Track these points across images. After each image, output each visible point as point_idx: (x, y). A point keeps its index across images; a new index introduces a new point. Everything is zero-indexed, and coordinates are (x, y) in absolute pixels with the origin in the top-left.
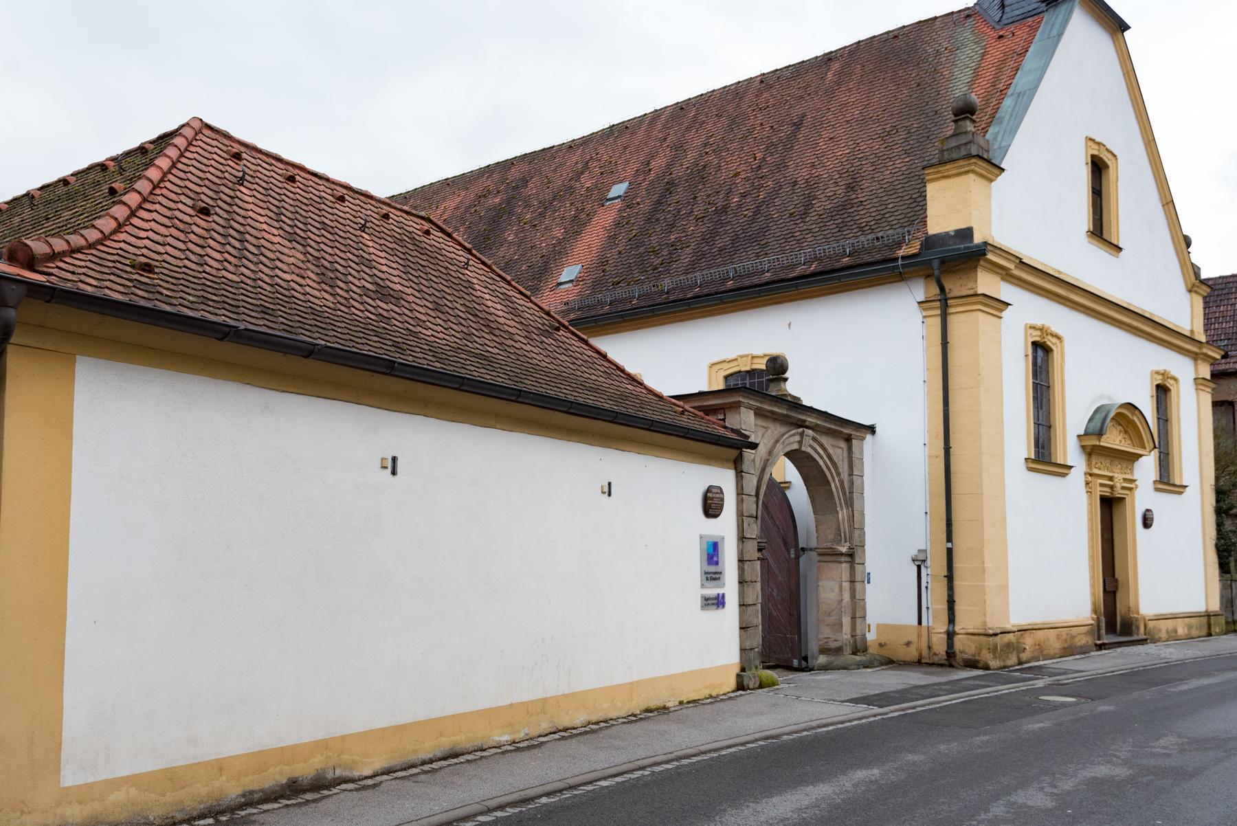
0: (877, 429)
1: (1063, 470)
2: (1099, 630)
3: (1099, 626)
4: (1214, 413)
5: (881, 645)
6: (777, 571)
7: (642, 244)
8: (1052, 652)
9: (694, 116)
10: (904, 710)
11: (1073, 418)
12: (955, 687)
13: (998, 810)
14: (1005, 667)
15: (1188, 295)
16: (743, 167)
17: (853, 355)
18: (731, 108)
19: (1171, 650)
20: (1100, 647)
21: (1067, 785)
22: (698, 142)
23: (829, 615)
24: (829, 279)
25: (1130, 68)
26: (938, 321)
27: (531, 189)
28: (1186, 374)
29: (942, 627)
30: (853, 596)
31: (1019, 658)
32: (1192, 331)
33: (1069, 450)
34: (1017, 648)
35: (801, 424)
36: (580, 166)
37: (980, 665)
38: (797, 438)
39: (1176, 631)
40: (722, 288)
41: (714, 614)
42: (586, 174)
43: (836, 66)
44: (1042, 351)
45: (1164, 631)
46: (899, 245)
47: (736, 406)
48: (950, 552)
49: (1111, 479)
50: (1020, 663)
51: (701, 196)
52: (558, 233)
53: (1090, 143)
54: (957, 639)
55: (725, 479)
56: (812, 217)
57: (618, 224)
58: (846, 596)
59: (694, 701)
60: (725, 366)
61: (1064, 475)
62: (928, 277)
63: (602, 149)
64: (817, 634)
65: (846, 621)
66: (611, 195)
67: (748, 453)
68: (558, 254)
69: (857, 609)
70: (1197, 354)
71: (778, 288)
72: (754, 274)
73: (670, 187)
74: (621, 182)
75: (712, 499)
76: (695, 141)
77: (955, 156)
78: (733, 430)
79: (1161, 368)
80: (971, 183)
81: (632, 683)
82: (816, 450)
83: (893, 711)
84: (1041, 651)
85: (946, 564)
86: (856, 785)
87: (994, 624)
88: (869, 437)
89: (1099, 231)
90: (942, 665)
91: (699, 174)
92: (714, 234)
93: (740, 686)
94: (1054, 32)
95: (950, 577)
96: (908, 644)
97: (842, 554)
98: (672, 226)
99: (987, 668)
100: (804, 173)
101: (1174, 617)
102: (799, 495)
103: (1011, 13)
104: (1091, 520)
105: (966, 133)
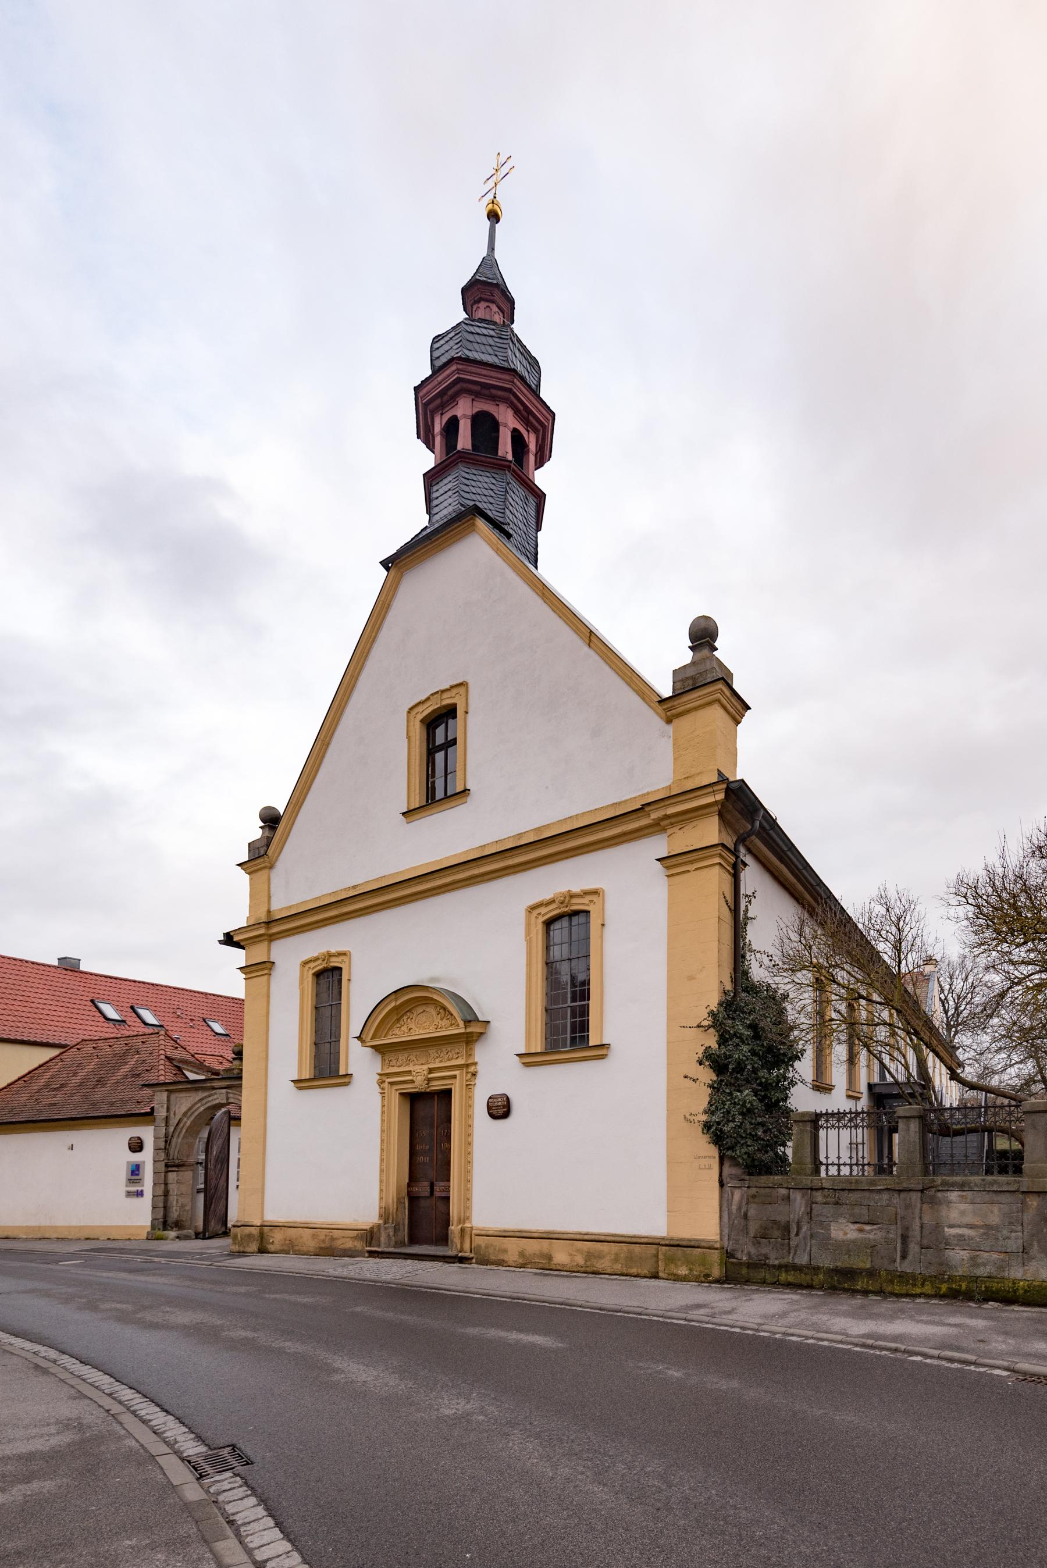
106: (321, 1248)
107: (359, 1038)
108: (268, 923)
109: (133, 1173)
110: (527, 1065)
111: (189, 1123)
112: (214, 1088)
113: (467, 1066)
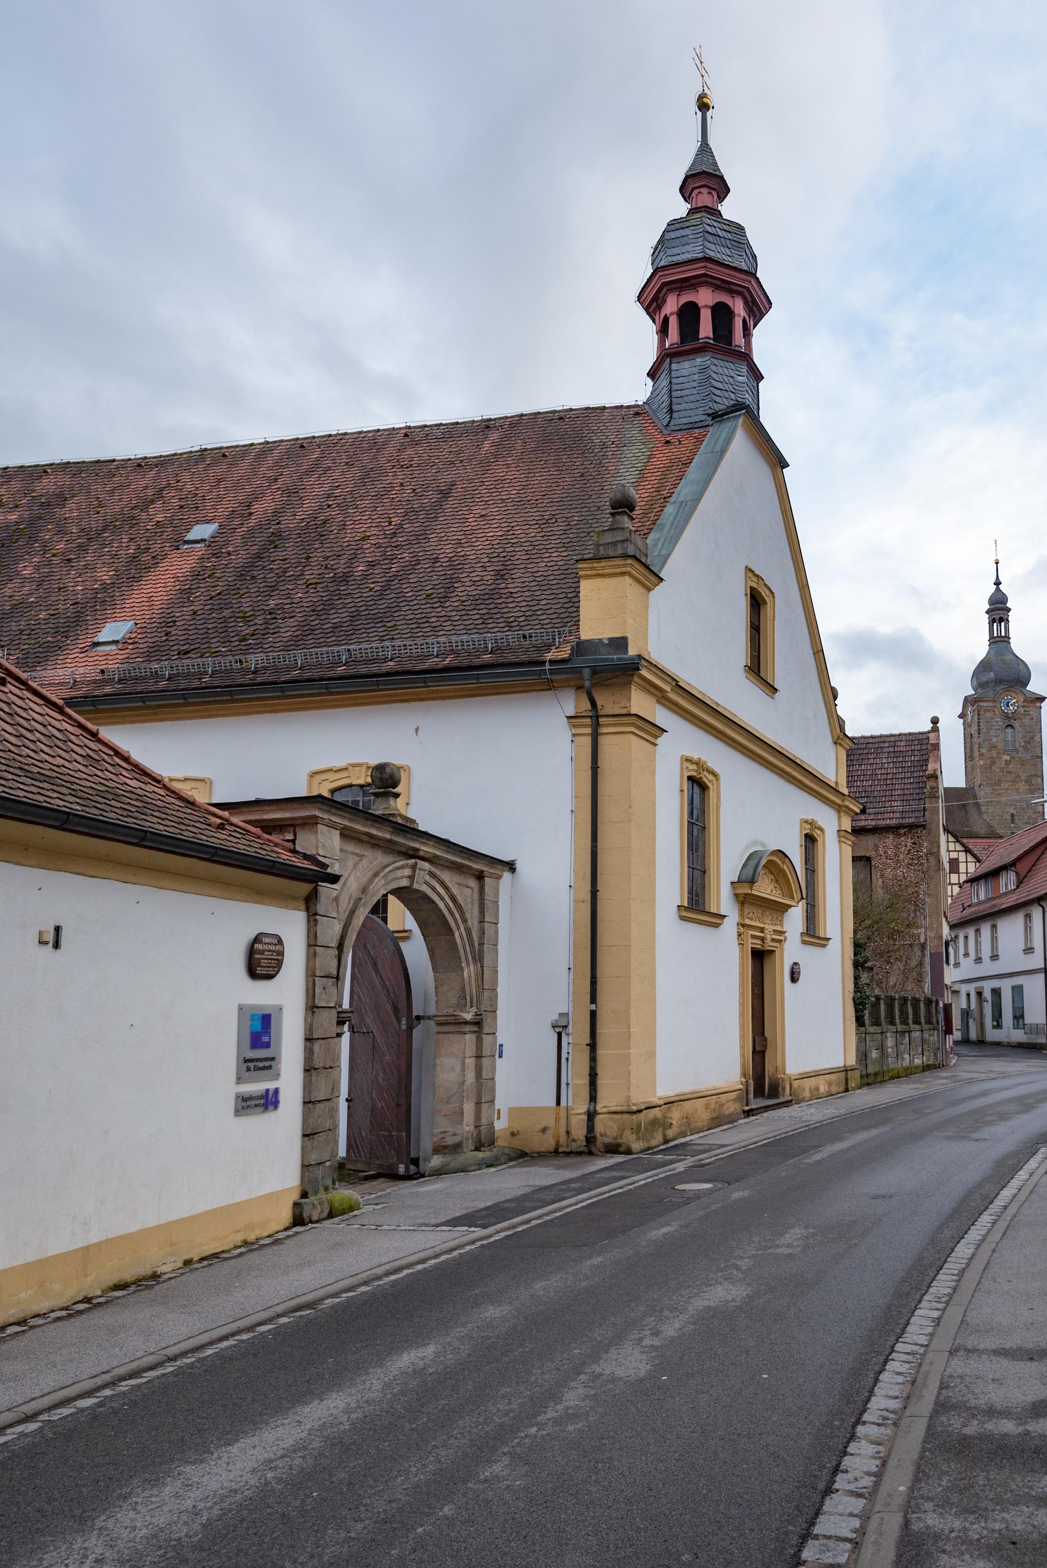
0: (518, 866)
1: (716, 920)
2: (747, 1094)
3: (747, 1091)
4: (854, 867)
5: (513, 1134)
6: (384, 1048)
7: (228, 605)
8: (700, 1124)
9: (317, 459)
10: (514, 1227)
11: (727, 864)
12: (587, 1183)
13: (573, 1397)
14: (649, 1148)
15: (834, 746)
16: (374, 531)
17: (489, 775)
18: (365, 458)
19: (813, 1110)
20: (748, 1113)
21: (671, 1329)
22: (319, 491)
23: (447, 1102)
24: (467, 678)
25: (788, 507)
26: (587, 741)
27: (71, 510)
28: (831, 823)
29: (583, 1107)
30: (479, 1075)
31: (664, 1136)
32: (837, 783)
33: (722, 898)
34: (662, 1124)
35: (413, 854)
36: (150, 492)
37: (622, 1149)
38: (407, 872)
39: (818, 1089)
40: (331, 674)
41: (258, 1122)
42: (158, 504)
43: (494, 436)
44: (698, 785)
45: (807, 1090)
46: (548, 647)
47: (311, 823)
48: (593, 1014)
49: (762, 930)
50: (666, 1142)
51: (317, 557)
52: (105, 574)
53: (750, 574)
54: (598, 1119)
55: (289, 926)
56: (453, 603)
57: (196, 575)
58: (470, 1076)
59: (215, 1256)
60: (331, 776)
61: (717, 926)
62: (579, 688)
63: (186, 476)
64: (433, 1125)
65: (469, 1108)
66: (190, 536)
67: (326, 890)
68: (103, 602)
69: (483, 1090)
70: (840, 806)
71: (402, 682)
72: (374, 661)
73: (276, 539)
74: (208, 522)
75: (262, 952)
76: (315, 490)
77: (611, 553)
78: (305, 856)
79: (809, 817)
80: (626, 587)
81: (87, 1248)
82: (434, 889)
83: (498, 1232)
84: (689, 1126)
85: (590, 1031)
86: (388, 1385)
87: (639, 1098)
88: (507, 875)
89: (756, 666)
90: (580, 1154)
91: (317, 529)
92: (328, 606)
93: (299, 1220)
94: (718, 448)
95: (593, 1046)
96: (544, 1130)
97: (466, 1023)
98: (274, 588)
99: (629, 1152)
100: (448, 550)
101: (817, 1074)
102: (416, 951)
103: (679, 420)
104: (742, 974)
105: (623, 529)
106: (713, 1119)
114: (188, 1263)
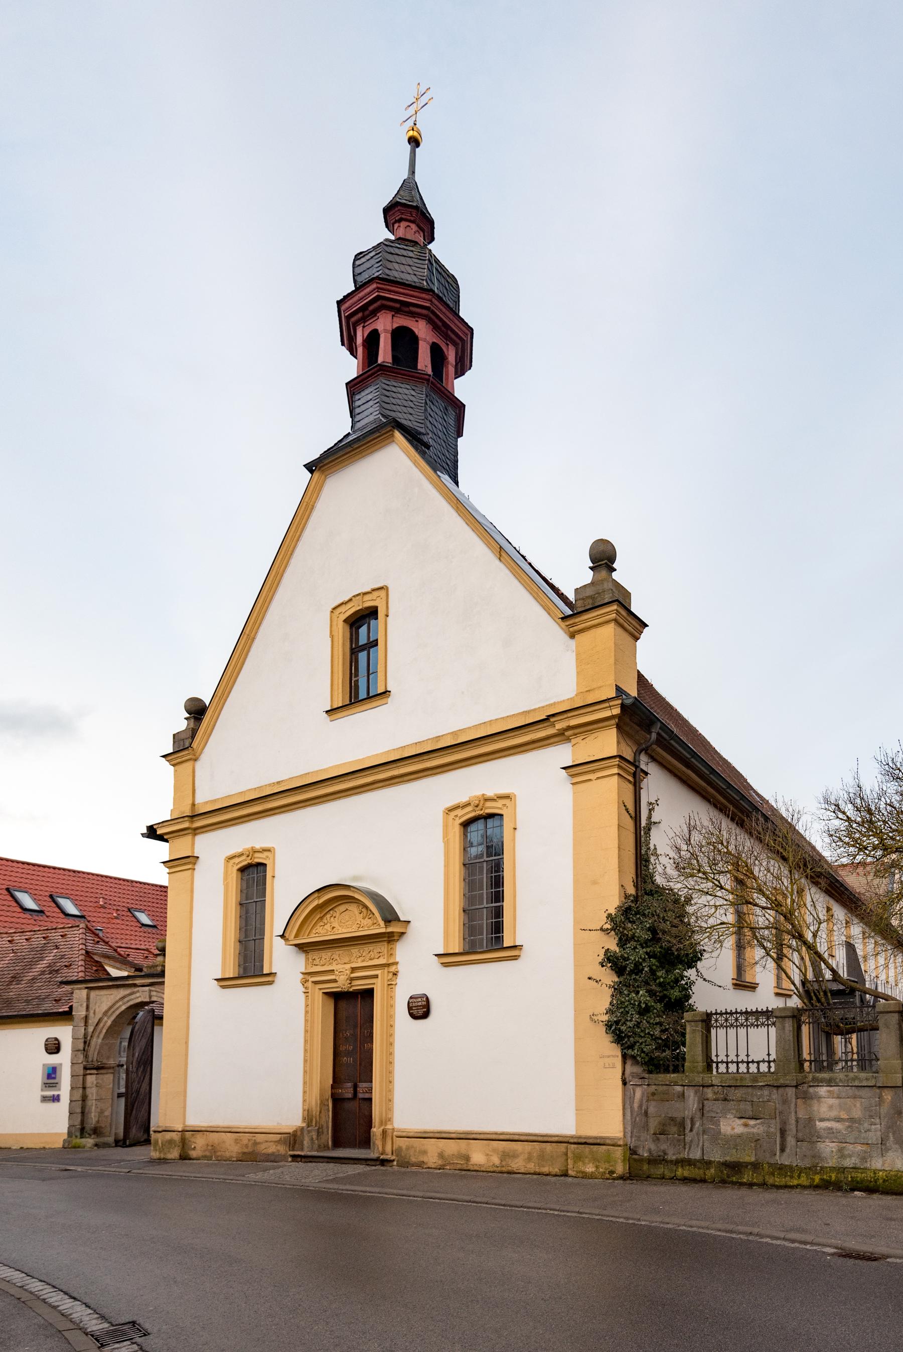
8: (227, 1154)
66: (137, 914)
106: (244, 1153)
107: (282, 936)
108: (192, 817)
109: (49, 1076)
110: (446, 965)
111: (109, 1023)
112: (135, 985)
113: (388, 965)
114: (22, 1148)
